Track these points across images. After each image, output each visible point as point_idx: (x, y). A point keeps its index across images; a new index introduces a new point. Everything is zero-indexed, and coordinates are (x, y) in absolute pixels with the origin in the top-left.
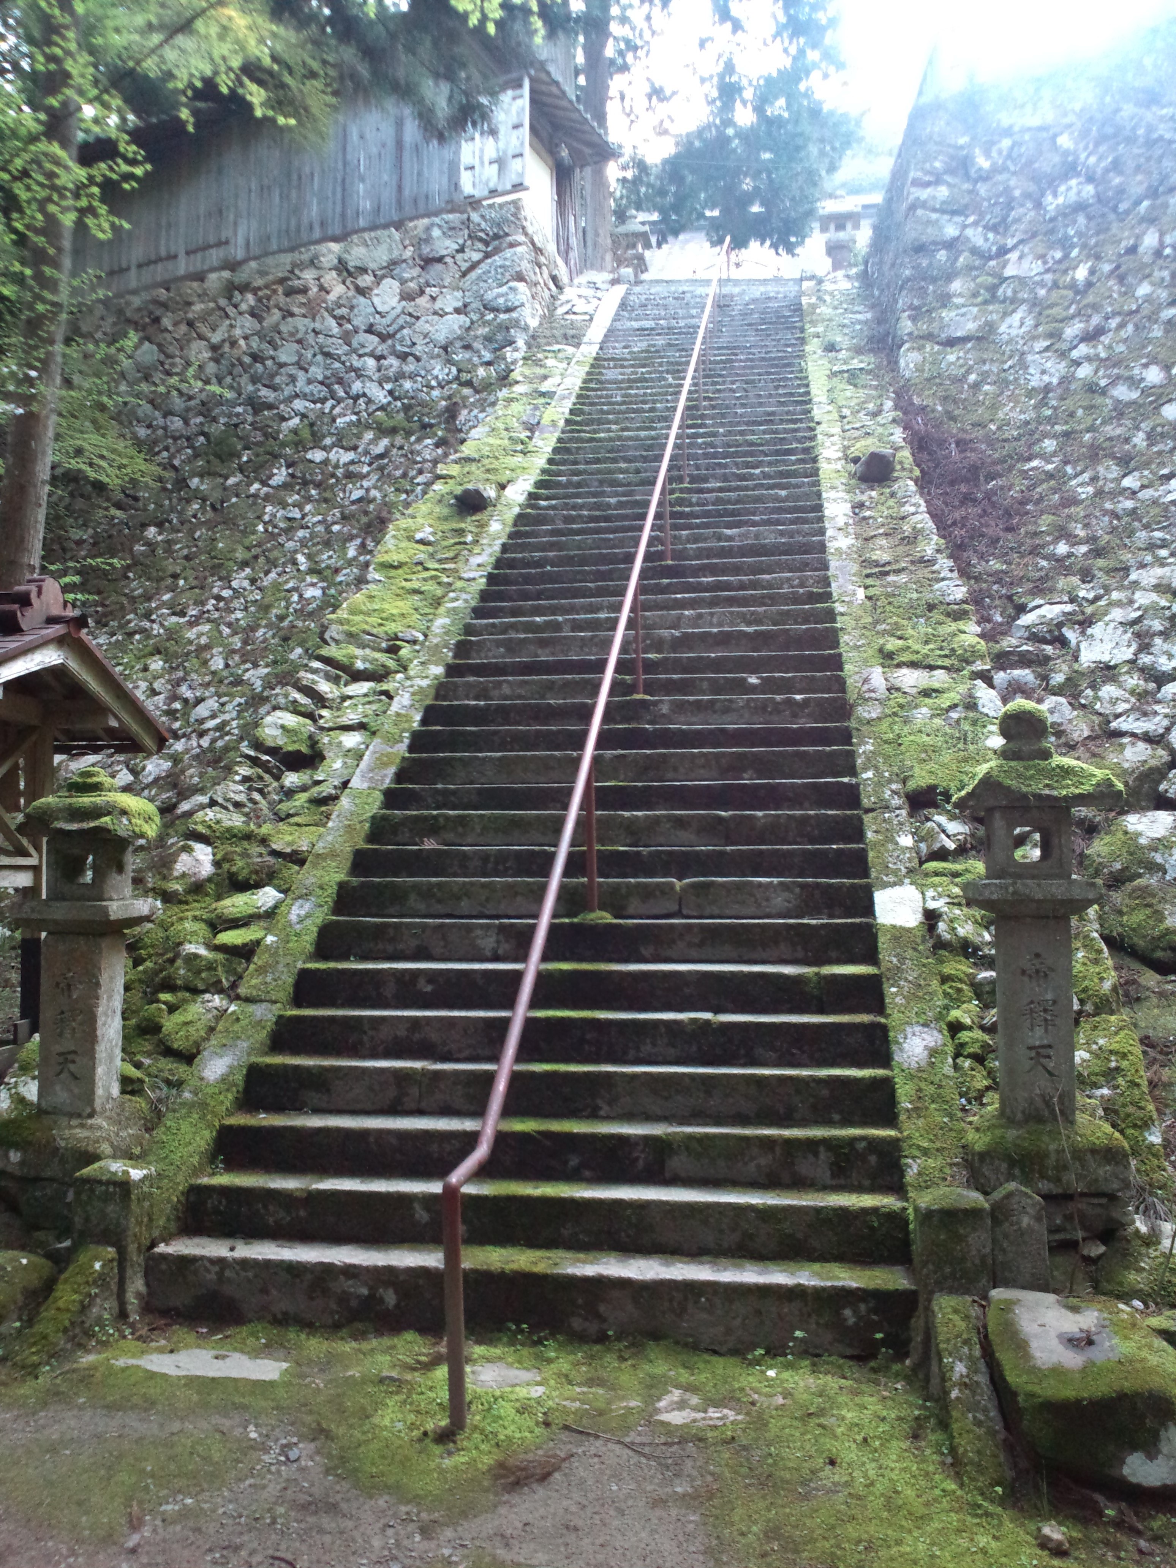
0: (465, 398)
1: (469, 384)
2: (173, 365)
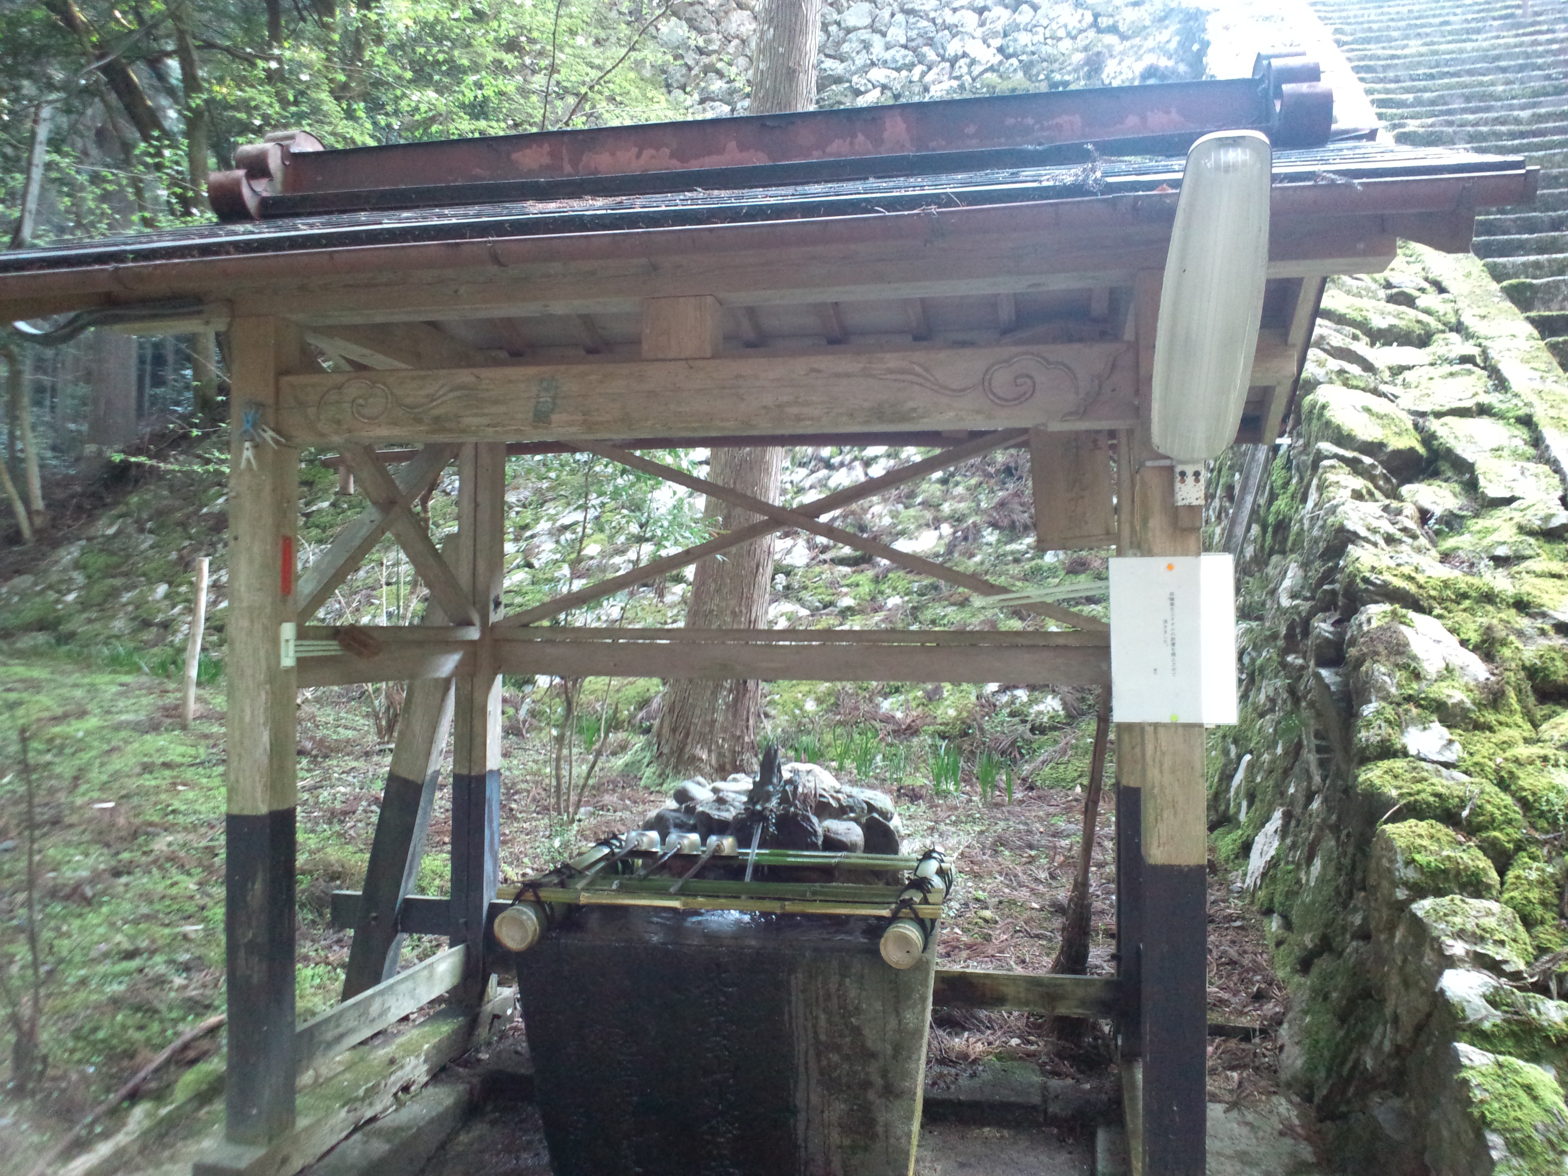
0: (1109, 47)
1: (1113, 29)
2: (708, 42)
